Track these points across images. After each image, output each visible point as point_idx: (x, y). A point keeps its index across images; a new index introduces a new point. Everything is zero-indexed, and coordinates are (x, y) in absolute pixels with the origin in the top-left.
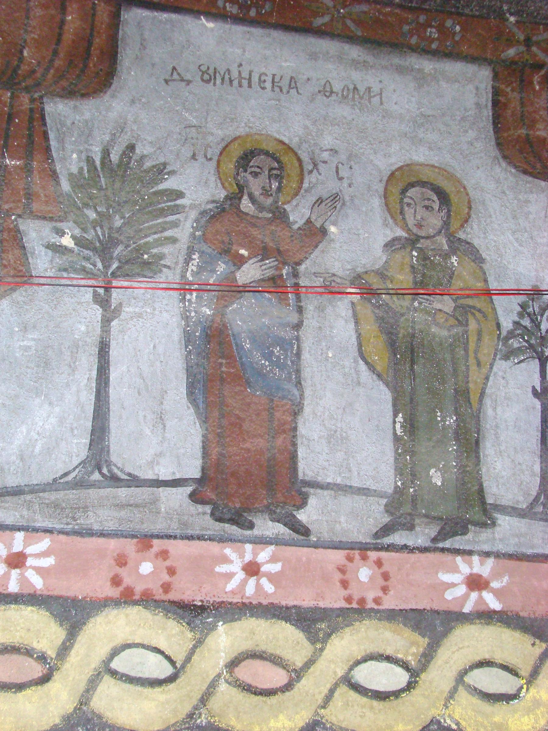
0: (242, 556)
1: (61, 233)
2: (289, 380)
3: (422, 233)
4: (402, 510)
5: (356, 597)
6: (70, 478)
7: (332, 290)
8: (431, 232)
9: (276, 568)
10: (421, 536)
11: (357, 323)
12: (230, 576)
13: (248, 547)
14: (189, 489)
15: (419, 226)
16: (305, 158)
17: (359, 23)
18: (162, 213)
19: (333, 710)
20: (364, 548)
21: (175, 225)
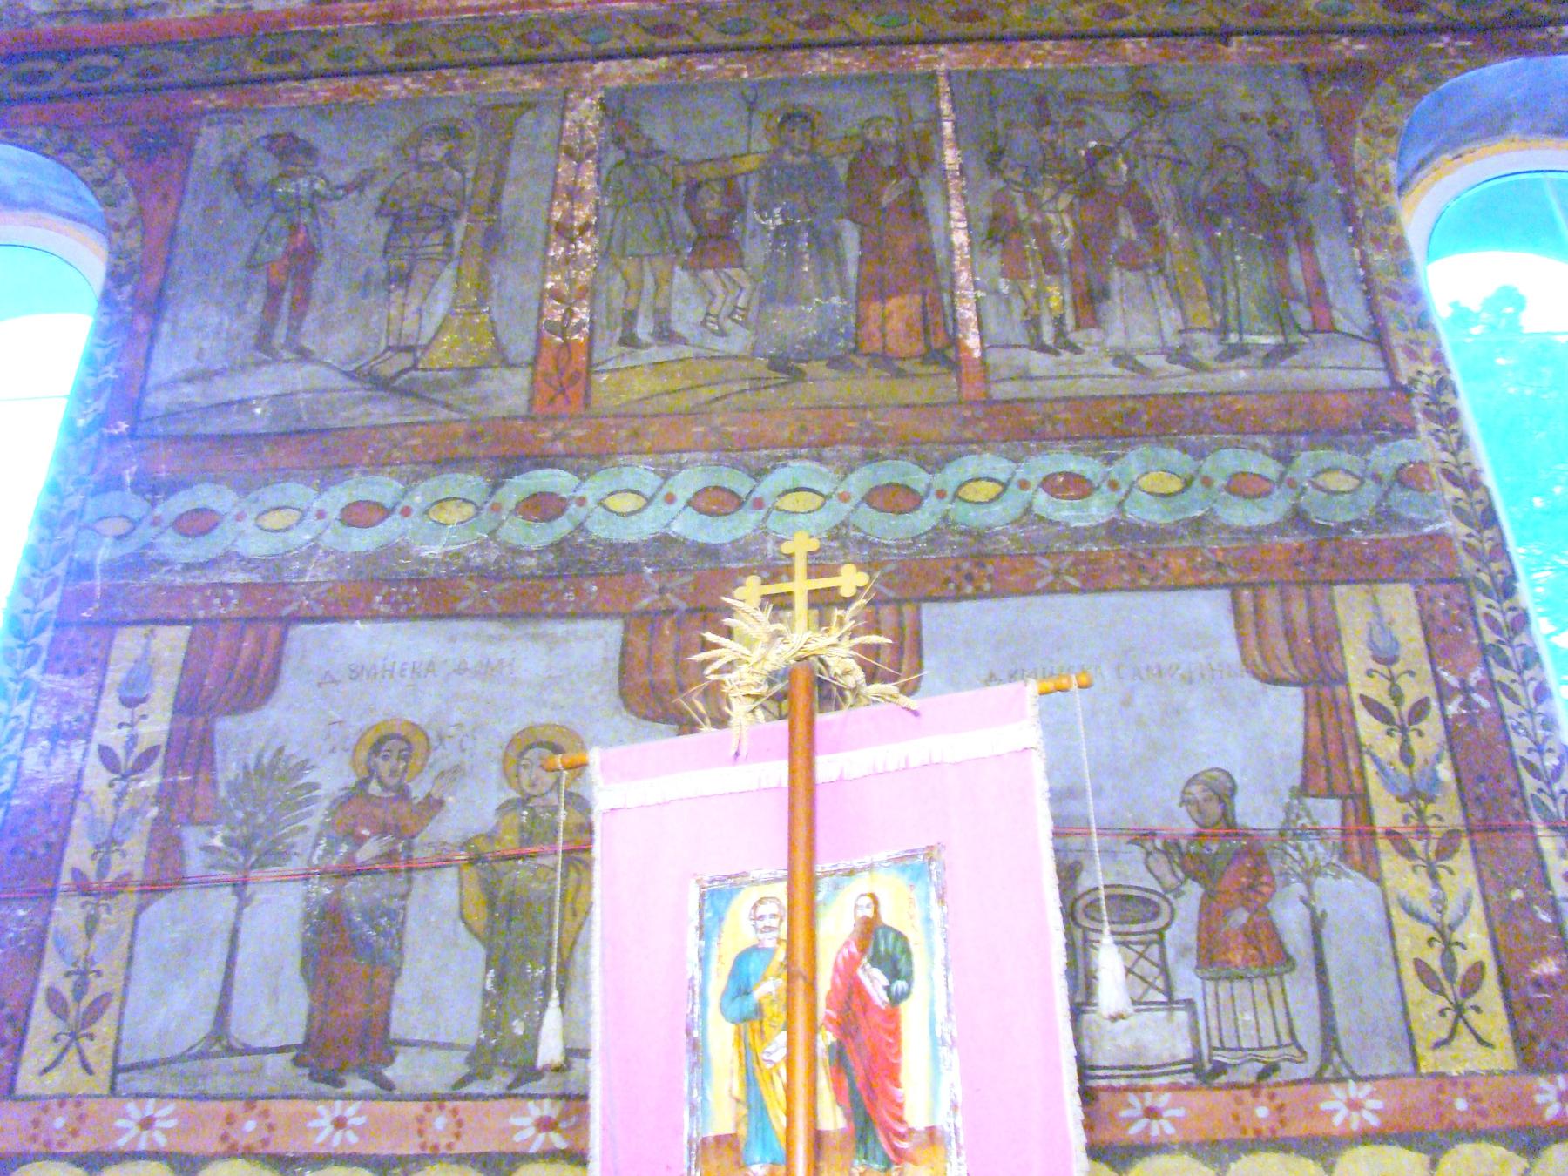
0: (332, 1111)
1: (212, 834)
2: (392, 947)
3: (535, 792)
4: (481, 1061)
5: (430, 1145)
6: (194, 1051)
7: (440, 864)
8: (544, 790)
9: (360, 1121)
10: (499, 1081)
11: (461, 887)
12: (319, 1130)
13: (339, 1103)
14: (292, 1054)
15: (533, 785)
16: (433, 735)
17: (500, 601)
18: (300, 805)
19: (494, 310)
20: (442, 1098)
21: (309, 814)
